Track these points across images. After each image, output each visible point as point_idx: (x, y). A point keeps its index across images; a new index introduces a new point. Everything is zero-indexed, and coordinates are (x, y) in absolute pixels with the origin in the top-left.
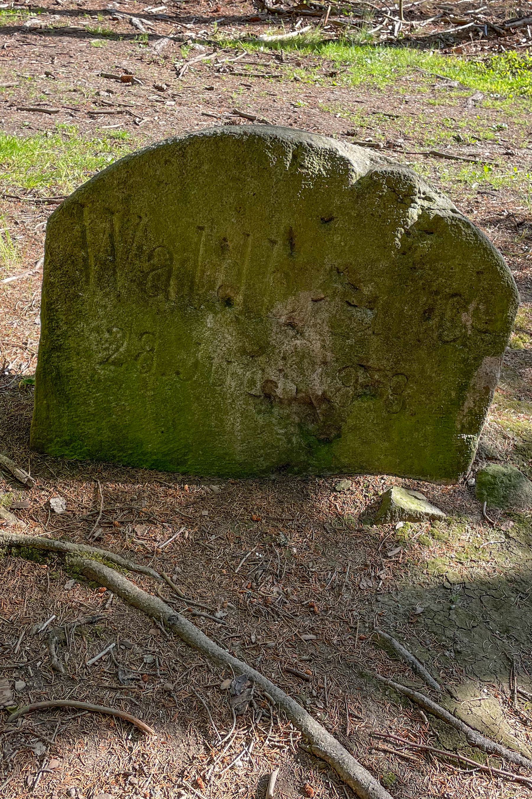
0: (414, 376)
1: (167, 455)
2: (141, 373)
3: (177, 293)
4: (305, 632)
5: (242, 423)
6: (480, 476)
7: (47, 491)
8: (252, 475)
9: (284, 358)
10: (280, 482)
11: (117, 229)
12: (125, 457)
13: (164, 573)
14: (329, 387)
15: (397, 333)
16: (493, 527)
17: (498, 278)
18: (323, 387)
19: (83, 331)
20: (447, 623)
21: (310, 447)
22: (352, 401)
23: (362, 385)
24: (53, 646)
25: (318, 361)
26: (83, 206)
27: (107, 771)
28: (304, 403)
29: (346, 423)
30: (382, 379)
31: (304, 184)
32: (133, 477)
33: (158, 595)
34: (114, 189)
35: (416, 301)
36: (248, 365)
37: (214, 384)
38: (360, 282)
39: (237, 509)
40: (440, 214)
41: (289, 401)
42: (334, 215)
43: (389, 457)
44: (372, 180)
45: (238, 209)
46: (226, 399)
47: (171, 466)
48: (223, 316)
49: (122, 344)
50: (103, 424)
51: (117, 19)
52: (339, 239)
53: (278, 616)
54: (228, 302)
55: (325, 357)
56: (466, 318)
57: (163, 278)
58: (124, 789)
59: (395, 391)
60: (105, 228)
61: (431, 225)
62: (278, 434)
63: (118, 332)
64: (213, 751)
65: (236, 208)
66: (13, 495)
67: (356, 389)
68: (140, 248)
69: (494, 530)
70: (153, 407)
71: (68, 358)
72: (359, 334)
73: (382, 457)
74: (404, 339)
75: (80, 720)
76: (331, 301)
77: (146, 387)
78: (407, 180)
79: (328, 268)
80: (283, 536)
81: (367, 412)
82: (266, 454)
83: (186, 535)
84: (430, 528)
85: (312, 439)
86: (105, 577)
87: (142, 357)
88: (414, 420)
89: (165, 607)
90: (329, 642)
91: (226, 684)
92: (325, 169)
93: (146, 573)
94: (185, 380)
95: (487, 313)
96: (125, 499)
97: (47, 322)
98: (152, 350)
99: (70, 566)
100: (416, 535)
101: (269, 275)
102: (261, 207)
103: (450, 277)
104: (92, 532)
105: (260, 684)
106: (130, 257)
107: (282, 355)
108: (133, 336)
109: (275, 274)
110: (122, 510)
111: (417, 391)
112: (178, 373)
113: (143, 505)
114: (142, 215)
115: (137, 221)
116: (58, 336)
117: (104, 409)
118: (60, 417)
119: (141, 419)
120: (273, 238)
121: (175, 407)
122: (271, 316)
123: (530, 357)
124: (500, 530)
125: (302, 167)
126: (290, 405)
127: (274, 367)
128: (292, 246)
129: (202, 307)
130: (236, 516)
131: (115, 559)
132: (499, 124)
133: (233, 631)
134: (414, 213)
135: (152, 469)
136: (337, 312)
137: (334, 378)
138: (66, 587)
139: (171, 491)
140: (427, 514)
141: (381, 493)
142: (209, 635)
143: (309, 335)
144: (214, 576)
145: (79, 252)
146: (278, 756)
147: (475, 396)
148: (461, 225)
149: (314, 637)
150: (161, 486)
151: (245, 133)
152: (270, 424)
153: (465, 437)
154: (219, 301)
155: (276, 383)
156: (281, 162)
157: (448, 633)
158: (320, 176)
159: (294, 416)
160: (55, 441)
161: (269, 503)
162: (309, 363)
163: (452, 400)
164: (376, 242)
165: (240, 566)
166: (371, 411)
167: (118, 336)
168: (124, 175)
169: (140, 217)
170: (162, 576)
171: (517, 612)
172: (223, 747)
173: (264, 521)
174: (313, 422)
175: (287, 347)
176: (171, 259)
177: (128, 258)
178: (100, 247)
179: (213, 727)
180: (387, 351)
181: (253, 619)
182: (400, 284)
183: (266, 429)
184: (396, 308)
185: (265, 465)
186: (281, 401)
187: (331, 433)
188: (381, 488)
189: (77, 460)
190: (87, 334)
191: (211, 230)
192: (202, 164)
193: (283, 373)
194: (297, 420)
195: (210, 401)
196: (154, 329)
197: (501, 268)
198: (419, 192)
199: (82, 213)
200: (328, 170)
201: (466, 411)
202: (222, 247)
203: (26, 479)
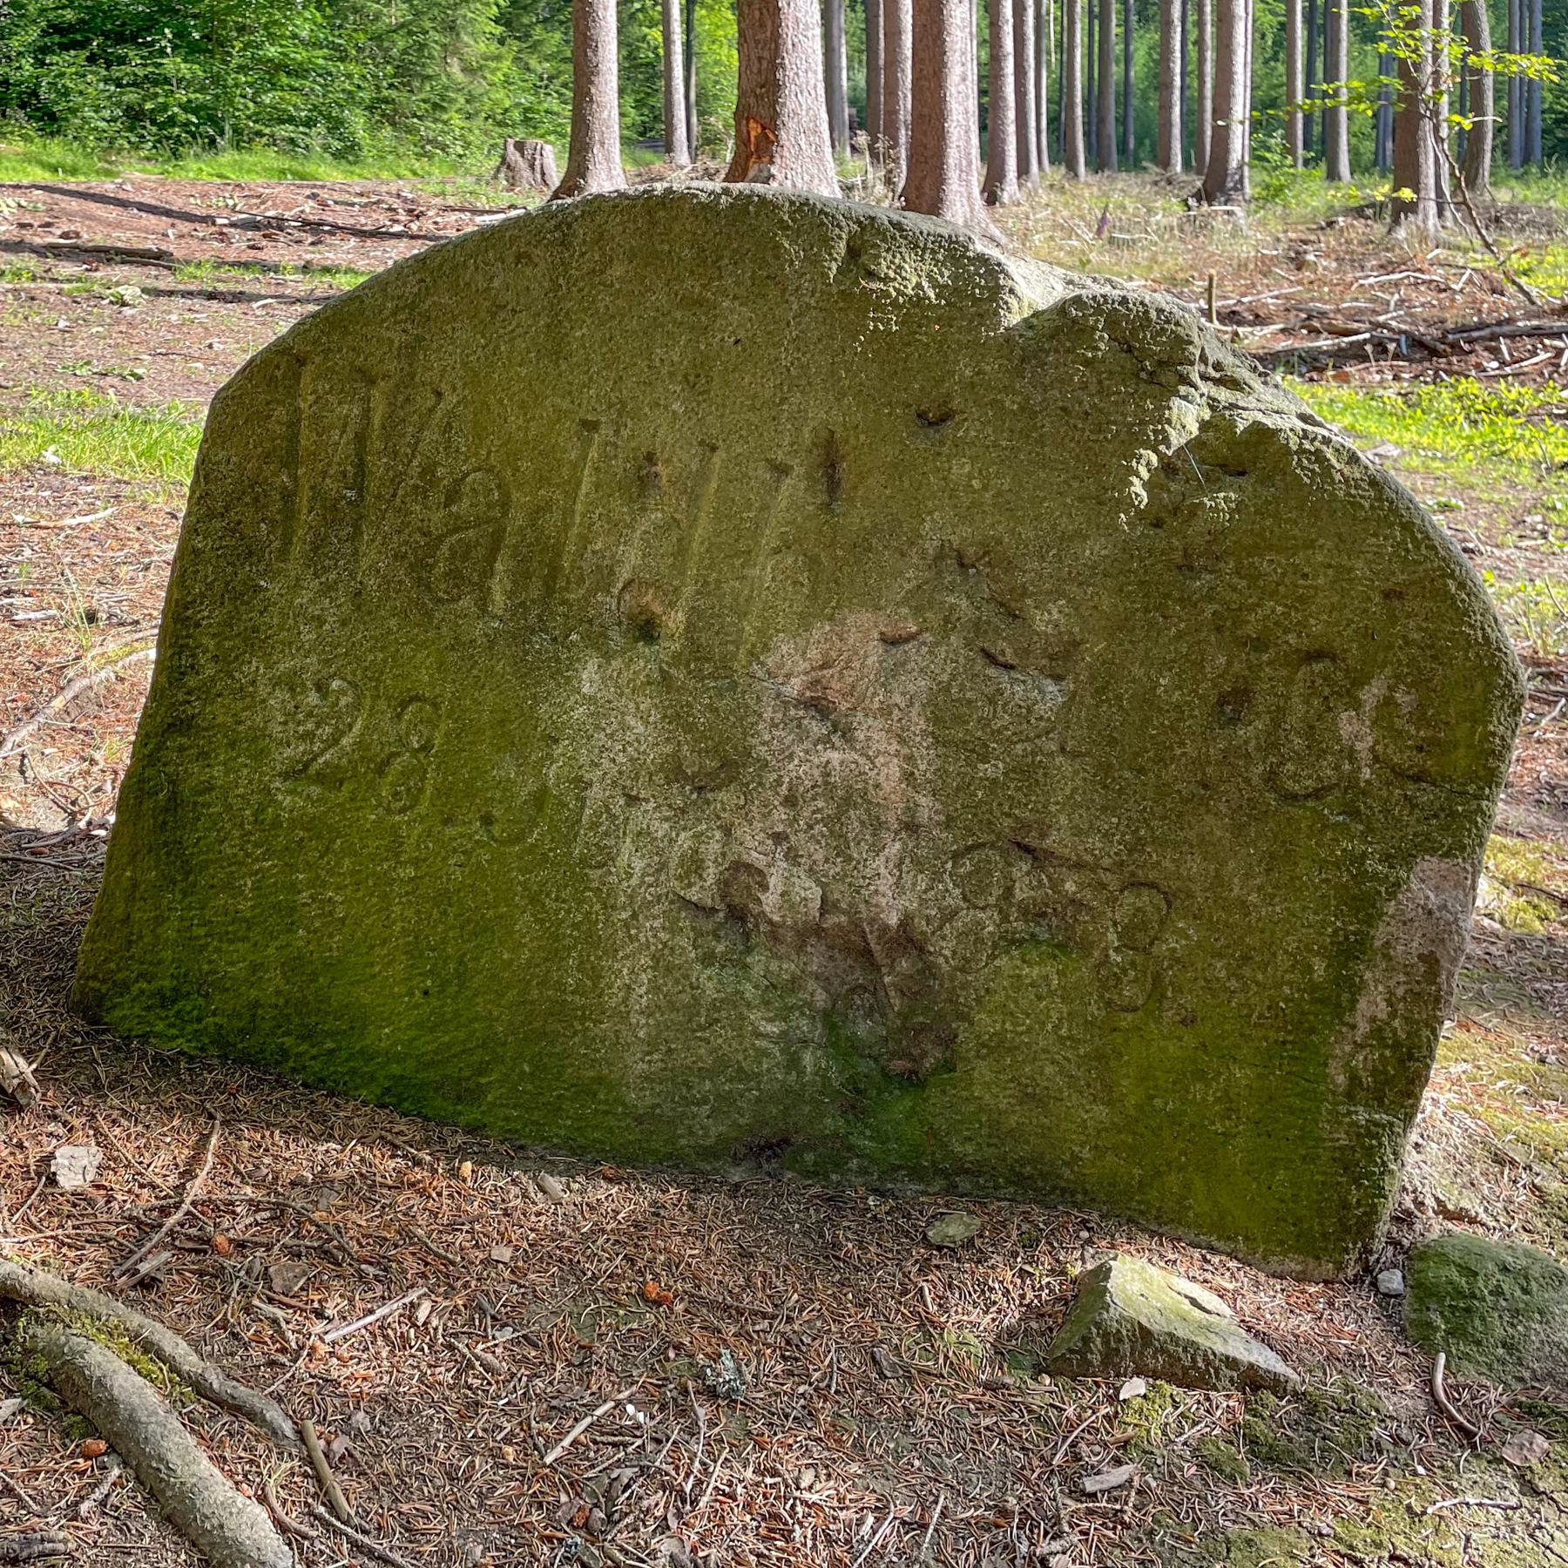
0: (1190, 895)
2: (389, 811)
3: (510, 595)
5: (654, 988)
6: (1419, 1265)
7: (65, 1124)
9: (790, 801)
10: (755, 1194)
11: (377, 421)
12: (314, 1058)
13: (309, 1424)
14: (923, 902)
15: (1137, 755)
16: (1474, 1447)
17: (1451, 613)
18: (903, 902)
22: (993, 957)
23: (1025, 912)
25: (891, 818)
26: (301, 361)
28: (847, 949)
29: (972, 1023)
30: (1088, 894)
31: (873, 319)
32: (321, 1118)
33: (263, 1499)
34: (383, 321)
35: (1194, 663)
36: (683, 812)
37: (584, 862)
38: (1025, 594)
40: (1269, 422)
42: (956, 404)
43: (1110, 1157)
44: (1066, 324)
45: (691, 378)
46: (613, 907)
47: (438, 1102)
48: (628, 667)
49: (350, 726)
50: (271, 951)
52: (967, 469)
54: (646, 630)
55: (912, 809)
56: (1349, 725)
59: (1128, 938)
60: (347, 416)
61: (1242, 454)
62: (759, 1035)
63: (345, 694)
65: (685, 377)
67: (1005, 918)
68: (428, 471)
69: (1478, 1456)
70: (410, 913)
71: (203, 755)
73: (1086, 1154)
74: (1158, 777)
76: (937, 644)
77: (397, 855)
78: (1168, 322)
79: (931, 547)
80: (730, 1364)
81: (1040, 998)
83: (422, 1314)
86: (112, 1402)
87: (397, 765)
88: (1190, 1040)
92: (934, 284)
94: (501, 843)
96: (276, 1179)
97: (170, 652)
98: (425, 748)
100: (1190, 1433)
101: (761, 559)
102: (754, 375)
103: (1301, 599)
104: (136, 1257)
106: (400, 492)
107: (784, 790)
108: (382, 705)
109: (778, 557)
110: (255, 1206)
111: (1199, 945)
112: (488, 821)
113: (323, 1203)
115: (429, 404)
117: (277, 907)
118: (160, 920)
119: (372, 947)
120: (780, 456)
121: (469, 921)
122: (760, 674)
123: (1564, 956)
124: (1501, 1460)
125: (871, 275)
126: (800, 948)
127: (758, 825)
128: (833, 486)
129: (574, 637)
130: (595, 1278)
131: (168, 1349)
132: (1443, 499)
134: (1187, 417)
135: (383, 1106)
136: (953, 677)
137: (937, 877)
139: (418, 1174)
140: (1231, 1363)
143: (869, 738)
144: (472, 1465)
145: (275, 475)
147: (1392, 983)
148: (1329, 453)
150: (393, 1157)
152: (735, 1000)
154: (620, 624)
155: (760, 872)
156: (814, 261)
158: (918, 301)
159: (811, 985)
160: (135, 989)
161: (709, 1251)
162: (862, 823)
163: (1314, 987)
164: (1075, 484)
165: (566, 1442)
166: (1052, 993)
167: (343, 702)
169: (439, 394)
170: (301, 1434)
173: (679, 1308)
174: (869, 1014)
175: (801, 769)
176: (505, 504)
177: (394, 496)
178: (329, 465)
180: (1104, 809)
182: (1147, 611)
183: (724, 1014)
184: (1134, 681)
185: (713, 1132)
187: (924, 1054)
188: (1077, 1254)
189: (182, 1053)
190: (263, 691)
191: (617, 432)
193: (785, 846)
194: (821, 998)
195: (568, 912)
196: (437, 691)
197: (1462, 585)
198: (1203, 359)
199: (297, 377)
200: (940, 286)
201: (1364, 1027)
203: (16, 1081)
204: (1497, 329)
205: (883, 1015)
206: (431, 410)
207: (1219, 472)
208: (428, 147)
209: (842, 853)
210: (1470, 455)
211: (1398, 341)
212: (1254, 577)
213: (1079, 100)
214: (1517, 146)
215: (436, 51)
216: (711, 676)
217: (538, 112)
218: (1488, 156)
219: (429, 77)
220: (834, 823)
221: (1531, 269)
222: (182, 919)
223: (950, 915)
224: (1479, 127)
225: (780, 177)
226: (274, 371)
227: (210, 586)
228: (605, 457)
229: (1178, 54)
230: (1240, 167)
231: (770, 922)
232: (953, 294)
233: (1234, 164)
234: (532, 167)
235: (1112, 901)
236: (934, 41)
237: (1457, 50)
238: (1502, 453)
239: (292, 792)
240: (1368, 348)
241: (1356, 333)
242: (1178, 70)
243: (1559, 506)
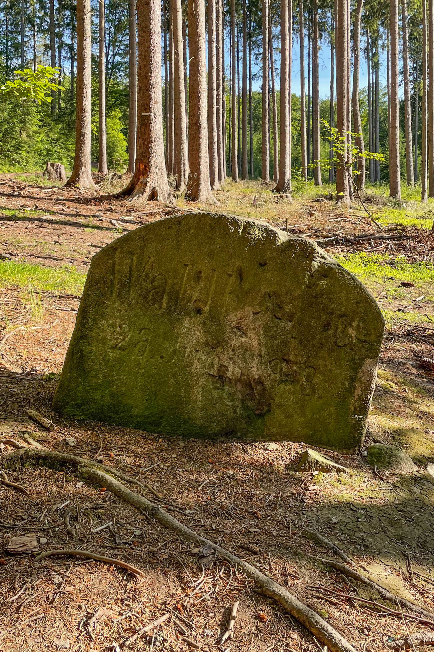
0: (320, 369)
1: (148, 417)
2: (137, 356)
3: (167, 304)
4: (251, 527)
5: (203, 395)
7: (63, 434)
8: (208, 437)
9: (233, 350)
11: (135, 264)
12: (118, 418)
14: (263, 372)
18: (259, 373)
19: (103, 326)
20: (356, 529)
21: (249, 418)
22: (278, 385)
24: (68, 519)
25: (256, 354)
26: (116, 249)
27: (108, 598)
28: (246, 385)
30: (298, 370)
37: (186, 366)
38: (283, 303)
39: (197, 455)
41: (236, 381)
43: (305, 430)
49: (127, 336)
50: (106, 392)
51: (102, 220)
53: (231, 516)
54: (199, 311)
56: (352, 331)
57: (160, 294)
58: (121, 608)
62: (227, 405)
64: (188, 591)
66: (39, 434)
67: (281, 376)
68: (147, 275)
70: (143, 381)
72: (283, 337)
73: (300, 429)
75: (87, 565)
76: (265, 314)
79: (263, 293)
81: (289, 394)
82: (219, 421)
84: (337, 477)
85: (250, 412)
87: (139, 345)
88: (321, 401)
89: (150, 503)
90: (270, 534)
91: (196, 550)
93: (134, 483)
95: (364, 328)
99: (80, 473)
105: (221, 553)
107: (232, 348)
108: (136, 330)
112: (162, 357)
114: (151, 256)
116: (86, 329)
118: (78, 386)
120: (230, 273)
124: (388, 482)
125: (249, 234)
126: (236, 385)
127: (226, 356)
128: (241, 279)
133: (199, 522)
134: (316, 264)
135: (136, 429)
137: (266, 366)
138: (77, 486)
141: (300, 452)
142: (182, 523)
146: (237, 596)
148: (344, 273)
149: (258, 530)
151: (217, 214)
153: (357, 417)
156: (236, 231)
157: (357, 535)
158: (259, 239)
159: (238, 393)
161: (220, 454)
163: (346, 388)
167: (126, 330)
168: (143, 233)
169: (150, 258)
171: (407, 529)
172: (195, 589)
176: (166, 283)
179: (187, 575)
181: (213, 517)
186: (230, 381)
187: (264, 408)
190: (105, 328)
192: (190, 229)
197: (371, 301)
198: (318, 253)
201: (356, 397)
202: (198, 277)
204: (370, 237)
205: (254, 400)
206: (148, 261)
207: (322, 277)
208: (13, 162)
209: (245, 361)
210: (365, 275)
211: (342, 240)
212: (330, 299)
213: (236, 156)
214: (372, 175)
215: (17, 129)
216: (215, 322)
217: (52, 151)
218: (364, 179)
219: (15, 139)
220: (244, 354)
221: (379, 218)
222: (83, 385)
223: (269, 376)
224: (361, 174)
225: (150, 182)
226: (108, 252)
227: (92, 303)
228: (190, 272)
229: (268, 143)
230: (289, 181)
231: (229, 379)
232: (267, 238)
233: (286, 180)
234: (57, 172)
235: (304, 371)
236: (197, 140)
237: (355, 151)
238: (374, 274)
239: (112, 352)
240: (334, 242)
241: (330, 237)
242: (268, 148)
243: (390, 289)
